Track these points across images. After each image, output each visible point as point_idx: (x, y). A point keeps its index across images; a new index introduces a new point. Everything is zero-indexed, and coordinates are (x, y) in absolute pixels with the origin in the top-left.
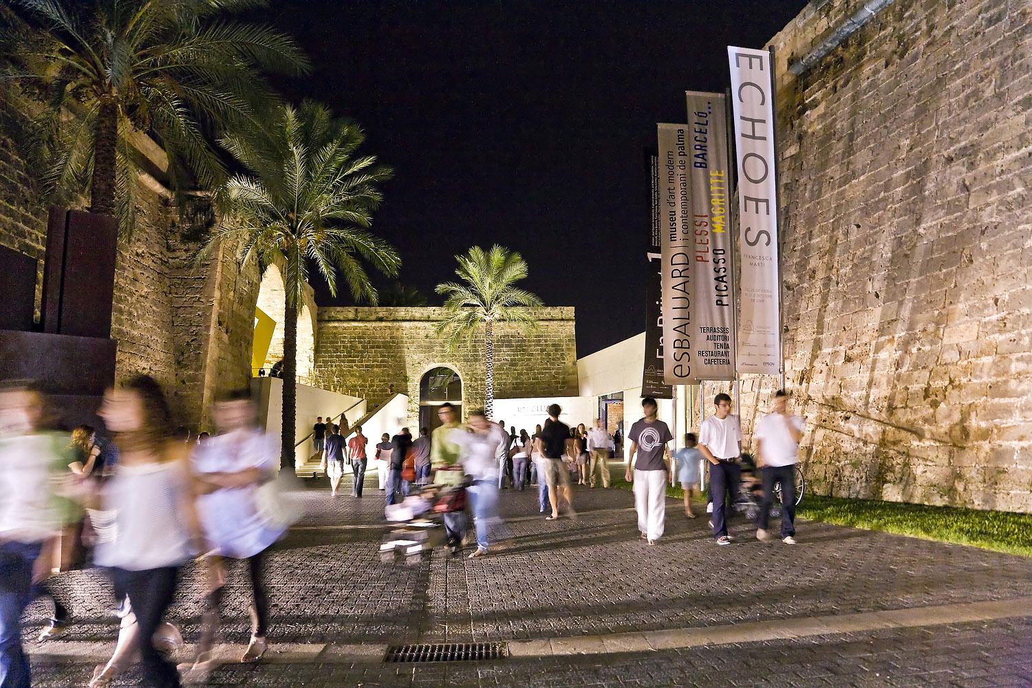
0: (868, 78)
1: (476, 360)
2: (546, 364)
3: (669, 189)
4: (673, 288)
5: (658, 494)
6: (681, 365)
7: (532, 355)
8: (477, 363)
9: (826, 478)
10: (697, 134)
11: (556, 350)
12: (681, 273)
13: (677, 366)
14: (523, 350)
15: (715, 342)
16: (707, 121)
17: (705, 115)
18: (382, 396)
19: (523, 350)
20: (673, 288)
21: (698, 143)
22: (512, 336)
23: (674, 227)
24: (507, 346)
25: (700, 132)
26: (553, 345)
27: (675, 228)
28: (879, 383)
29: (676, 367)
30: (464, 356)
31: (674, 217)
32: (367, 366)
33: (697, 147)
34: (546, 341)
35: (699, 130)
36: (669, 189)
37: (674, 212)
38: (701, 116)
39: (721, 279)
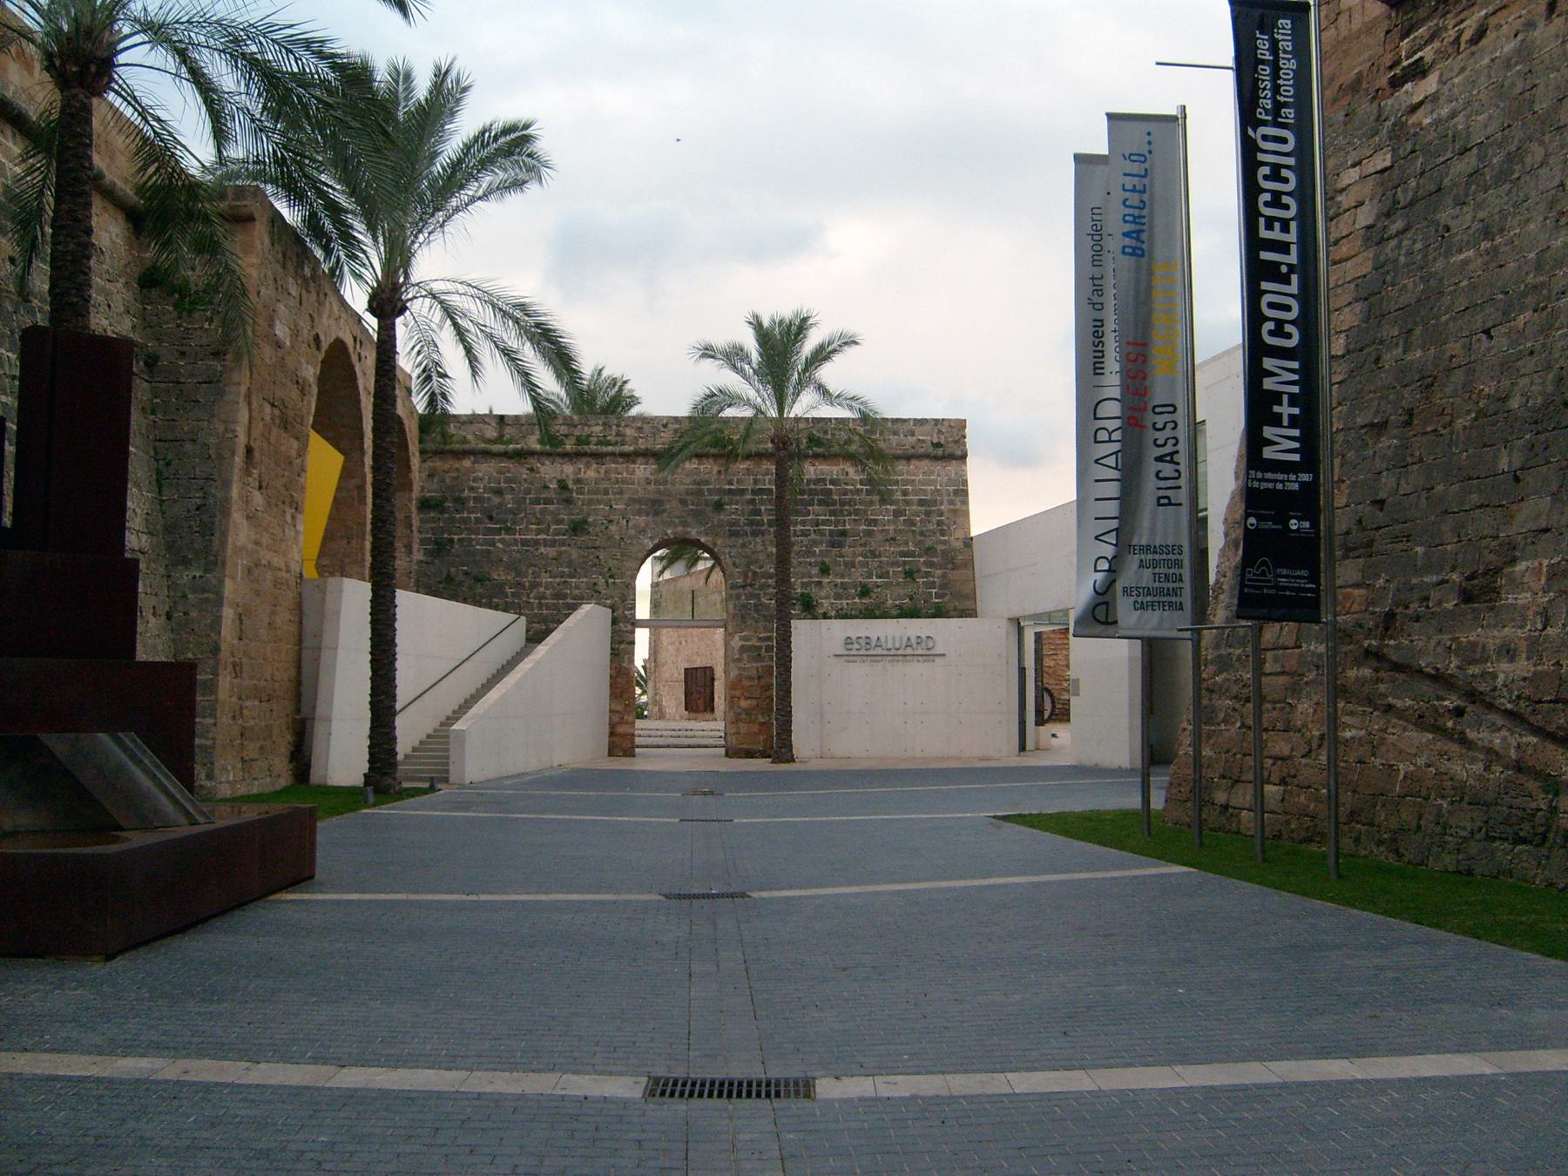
0: (1516, 36)
1: (755, 534)
2: (906, 543)
3: (1093, 278)
4: (1096, 461)
5: (237, 913)
6: (1107, 603)
7: (875, 522)
8: (758, 540)
9: (1419, 827)
10: (1128, 195)
11: (928, 514)
12: (1110, 434)
13: (1100, 604)
14: (856, 512)
15: (1156, 571)
16: (1146, 170)
17: (1143, 159)
18: (556, 607)
19: (856, 512)
20: (1096, 461)
21: (1128, 211)
22: (833, 482)
23: (1100, 348)
24: (821, 503)
25: (1134, 190)
26: (921, 503)
27: (1102, 351)
28: (1515, 650)
29: (1097, 605)
30: (732, 524)
31: (1100, 329)
32: (524, 543)
33: (1127, 218)
34: (905, 493)
35: (1131, 187)
36: (1093, 278)
37: (1102, 321)
38: (1134, 161)
39: (1168, 458)
